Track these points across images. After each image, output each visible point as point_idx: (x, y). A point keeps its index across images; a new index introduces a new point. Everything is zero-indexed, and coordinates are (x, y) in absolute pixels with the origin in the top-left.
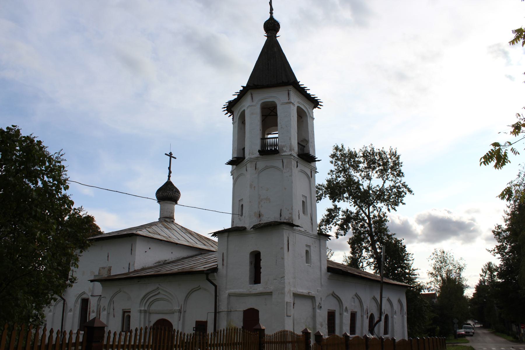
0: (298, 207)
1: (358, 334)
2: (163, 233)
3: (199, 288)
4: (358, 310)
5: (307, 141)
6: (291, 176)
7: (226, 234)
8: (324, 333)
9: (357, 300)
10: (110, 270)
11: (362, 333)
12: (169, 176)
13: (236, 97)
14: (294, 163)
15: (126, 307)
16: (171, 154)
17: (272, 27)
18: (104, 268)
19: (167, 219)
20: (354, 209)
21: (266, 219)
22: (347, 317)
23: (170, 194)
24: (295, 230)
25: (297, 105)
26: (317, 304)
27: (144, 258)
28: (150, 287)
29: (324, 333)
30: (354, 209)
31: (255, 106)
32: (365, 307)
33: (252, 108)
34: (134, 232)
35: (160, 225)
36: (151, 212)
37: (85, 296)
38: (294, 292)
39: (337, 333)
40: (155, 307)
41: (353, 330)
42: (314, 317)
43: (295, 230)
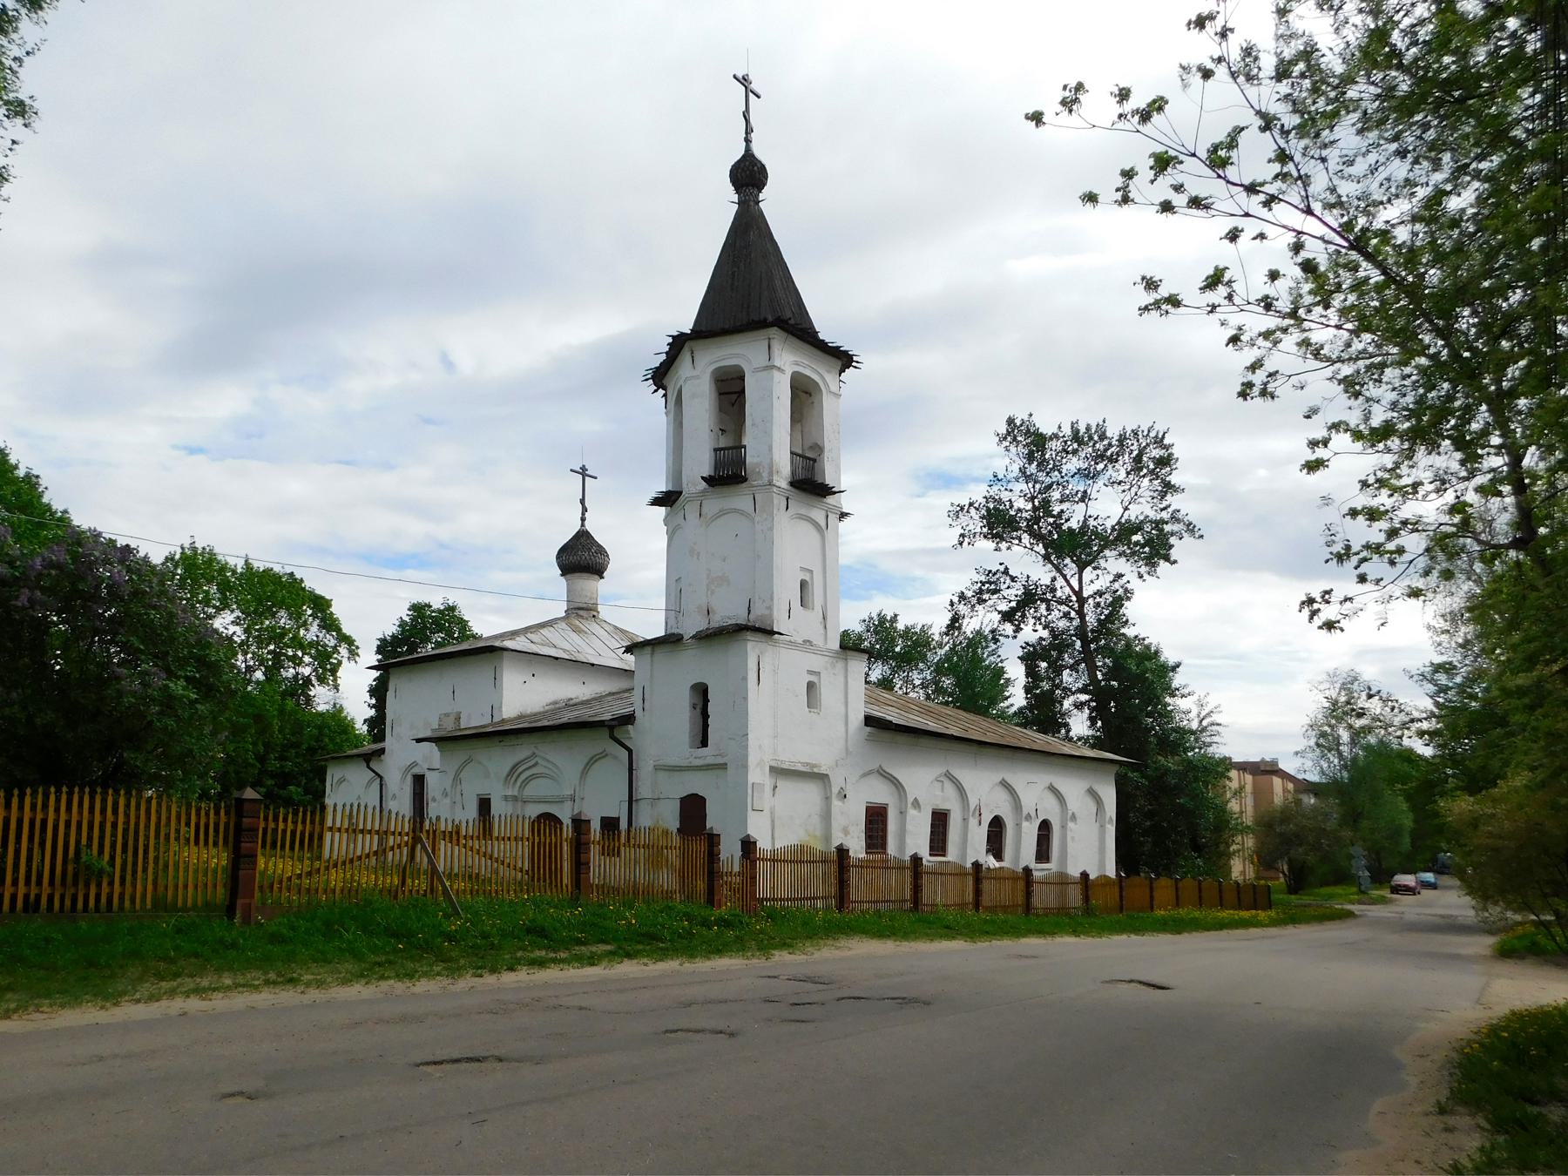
0: (785, 591)
1: (952, 855)
2: (564, 642)
3: (603, 755)
4: (950, 802)
5: (819, 448)
6: (771, 529)
7: (648, 649)
8: (857, 847)
9: (948, 786)
10: (458, 719)
11: (964, 855)
12: (583, 519)
13: (664, 357)
14: (779, 502)
15: (483, 789)
16: (584, 468)
17: (749, 176)
18: (447, 715)
19: (580, 611)
20: (1042, 574)
21: (718, 620)
22: (1030, 832)
23: (585, 556)
24: (776, 641)
25: (789, 371)
26: (835, 790)
27: (522, 695)
28: (522, 751)
29: (857, 847)
30: (1042, 574)
31: (697, 377)
32: (973, 803)
33: (697, 376)
34: (497, 644)
35: (563, 625)
36: (549, 594)
37: (416, 771)
38: (774, 764)
39: (892, 849)
40: (532, 790)
41: (938, 842)
42: (827, 816)
43: (776, 641)
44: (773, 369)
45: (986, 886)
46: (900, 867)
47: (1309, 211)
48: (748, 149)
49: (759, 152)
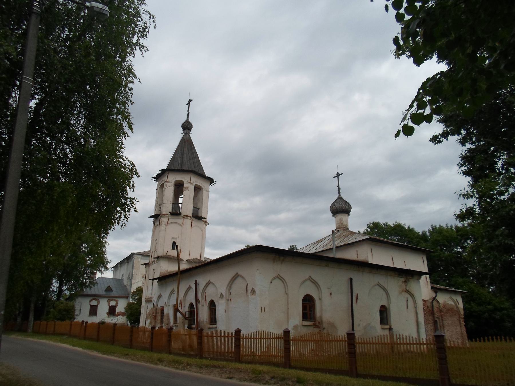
17: (187, 127)
44: (190, 182)
45: (243, 342)
46: (227, 336)
47: (25, 34)
48: (188, 119)
49: (190, 120)
